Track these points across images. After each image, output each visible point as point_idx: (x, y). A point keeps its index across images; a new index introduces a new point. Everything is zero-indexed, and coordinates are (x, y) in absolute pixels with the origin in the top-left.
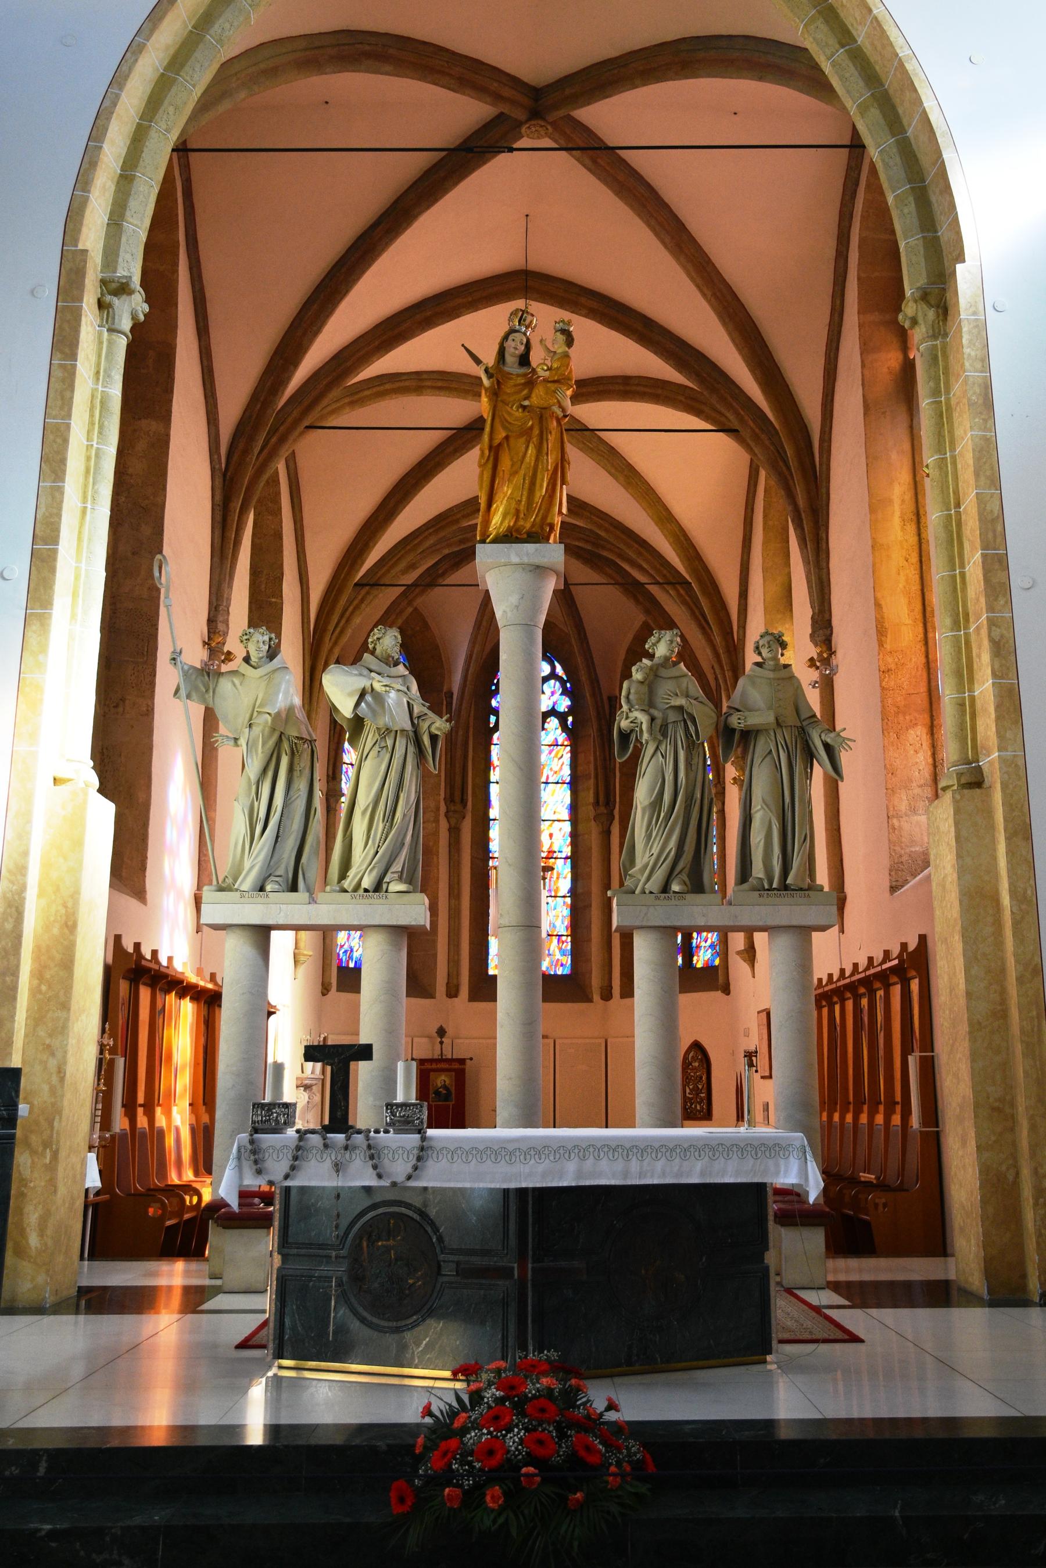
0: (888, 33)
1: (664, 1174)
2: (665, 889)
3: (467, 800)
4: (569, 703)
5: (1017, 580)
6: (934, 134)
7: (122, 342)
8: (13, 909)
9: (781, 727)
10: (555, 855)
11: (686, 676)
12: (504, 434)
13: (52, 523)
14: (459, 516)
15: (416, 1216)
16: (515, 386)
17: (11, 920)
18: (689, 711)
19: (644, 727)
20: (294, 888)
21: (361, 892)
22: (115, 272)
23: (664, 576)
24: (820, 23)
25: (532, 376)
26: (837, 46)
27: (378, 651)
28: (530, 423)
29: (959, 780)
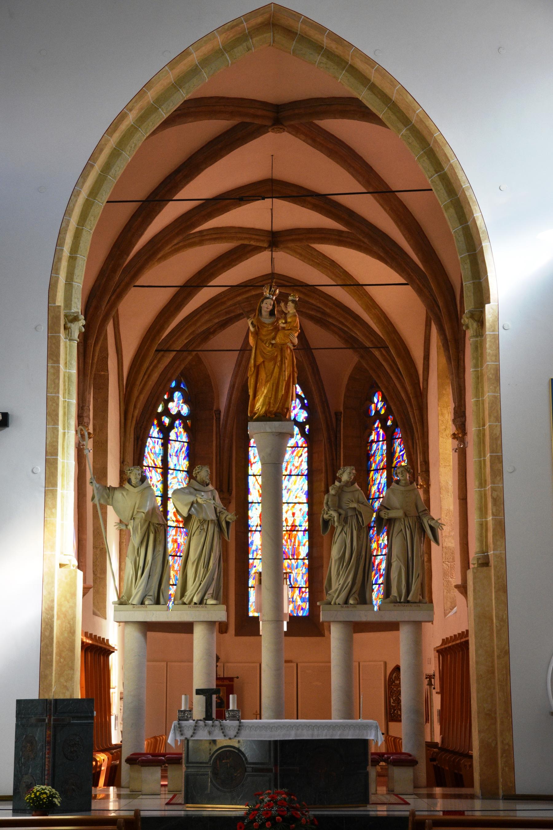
0: (458, 174)
1: (326, 736)
2: (346, 602)
3: (232, 490)
4: (306, 415)
5: (507, 467)
6: (479, 232)
7: (75, 344)
8: (49, 626)
9: (408, 517)
10: (297, 529)
11: (357, 490)
12: (262, 360)
13: (54, 446)
14: (225, 299)
15: (237, 751)
16: (268, 331)
17: (48, 631)
18: (359, 510)
19: (336, 519)
20: (158, 602)
21: (193, 603)
22: (71, 310)
23: (372, 341)
24: (425, 158)
25: (277, 324)
26: (434, 172)
27: (198, 478)
28: (276, 354)
29: (478, 562)
